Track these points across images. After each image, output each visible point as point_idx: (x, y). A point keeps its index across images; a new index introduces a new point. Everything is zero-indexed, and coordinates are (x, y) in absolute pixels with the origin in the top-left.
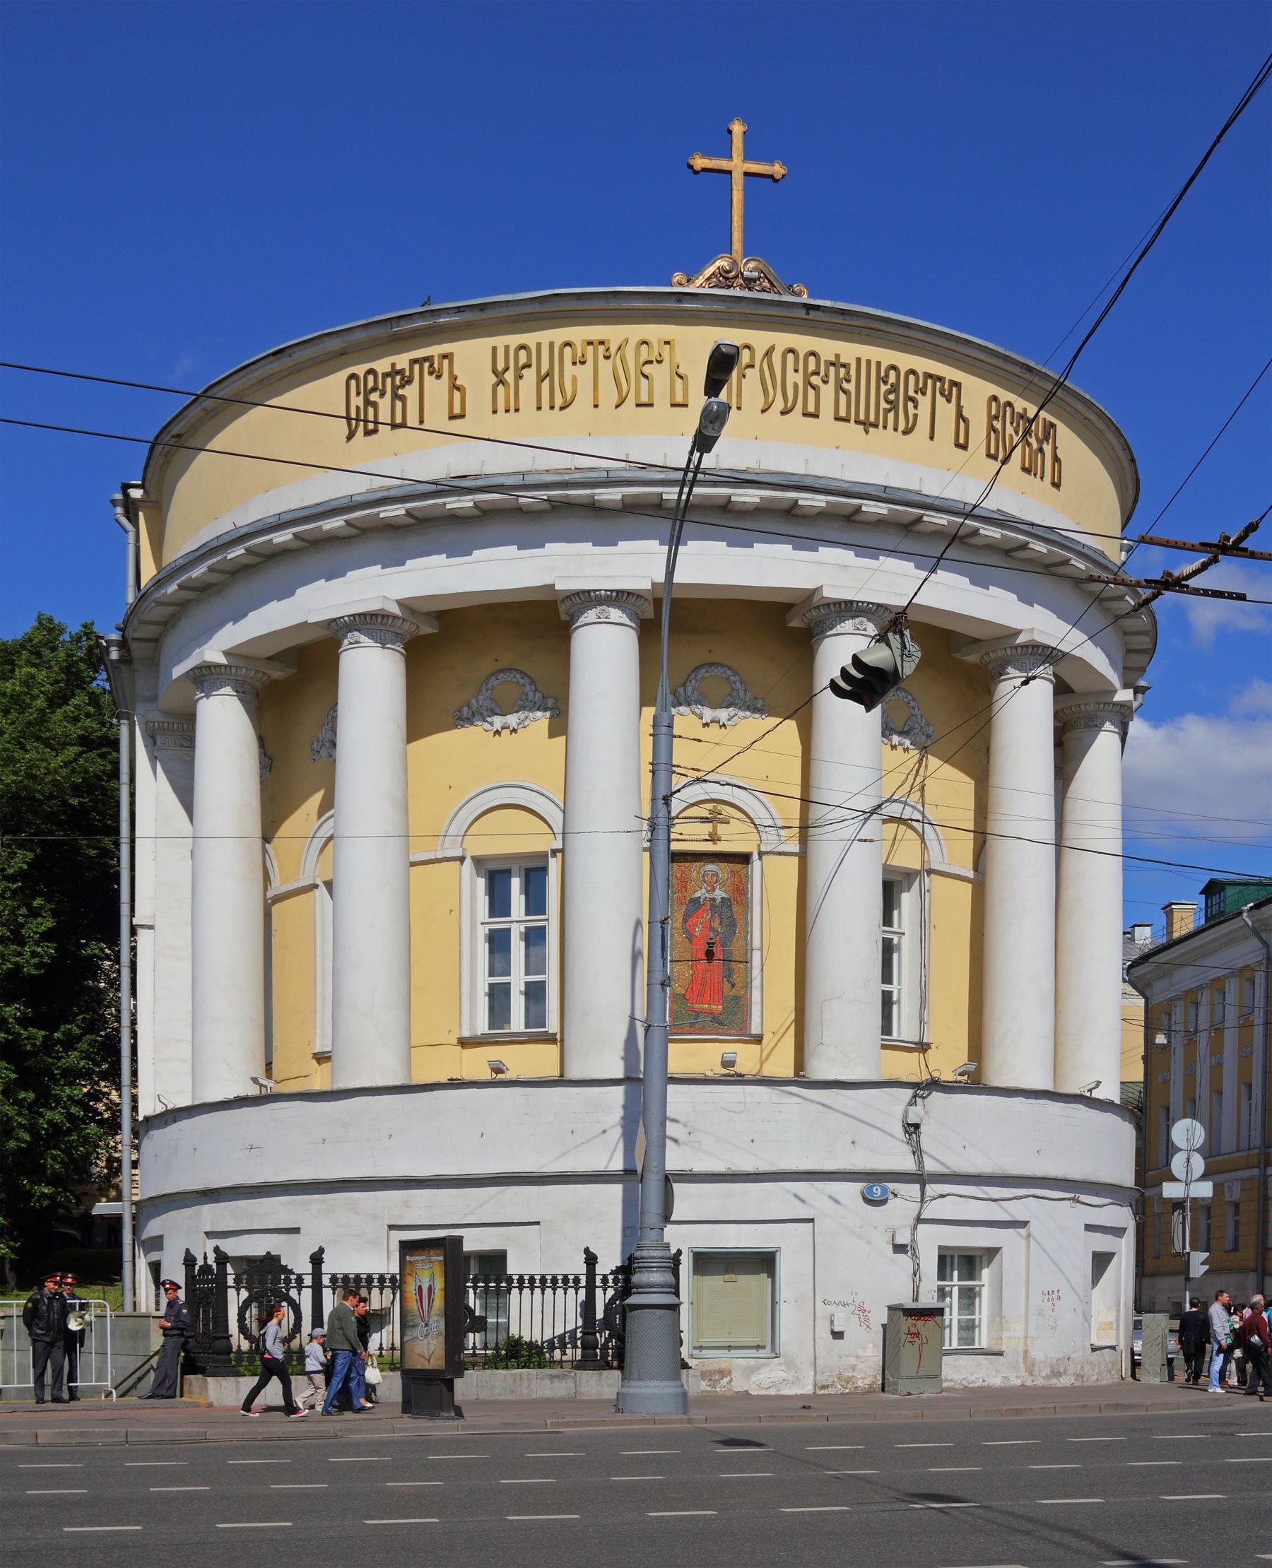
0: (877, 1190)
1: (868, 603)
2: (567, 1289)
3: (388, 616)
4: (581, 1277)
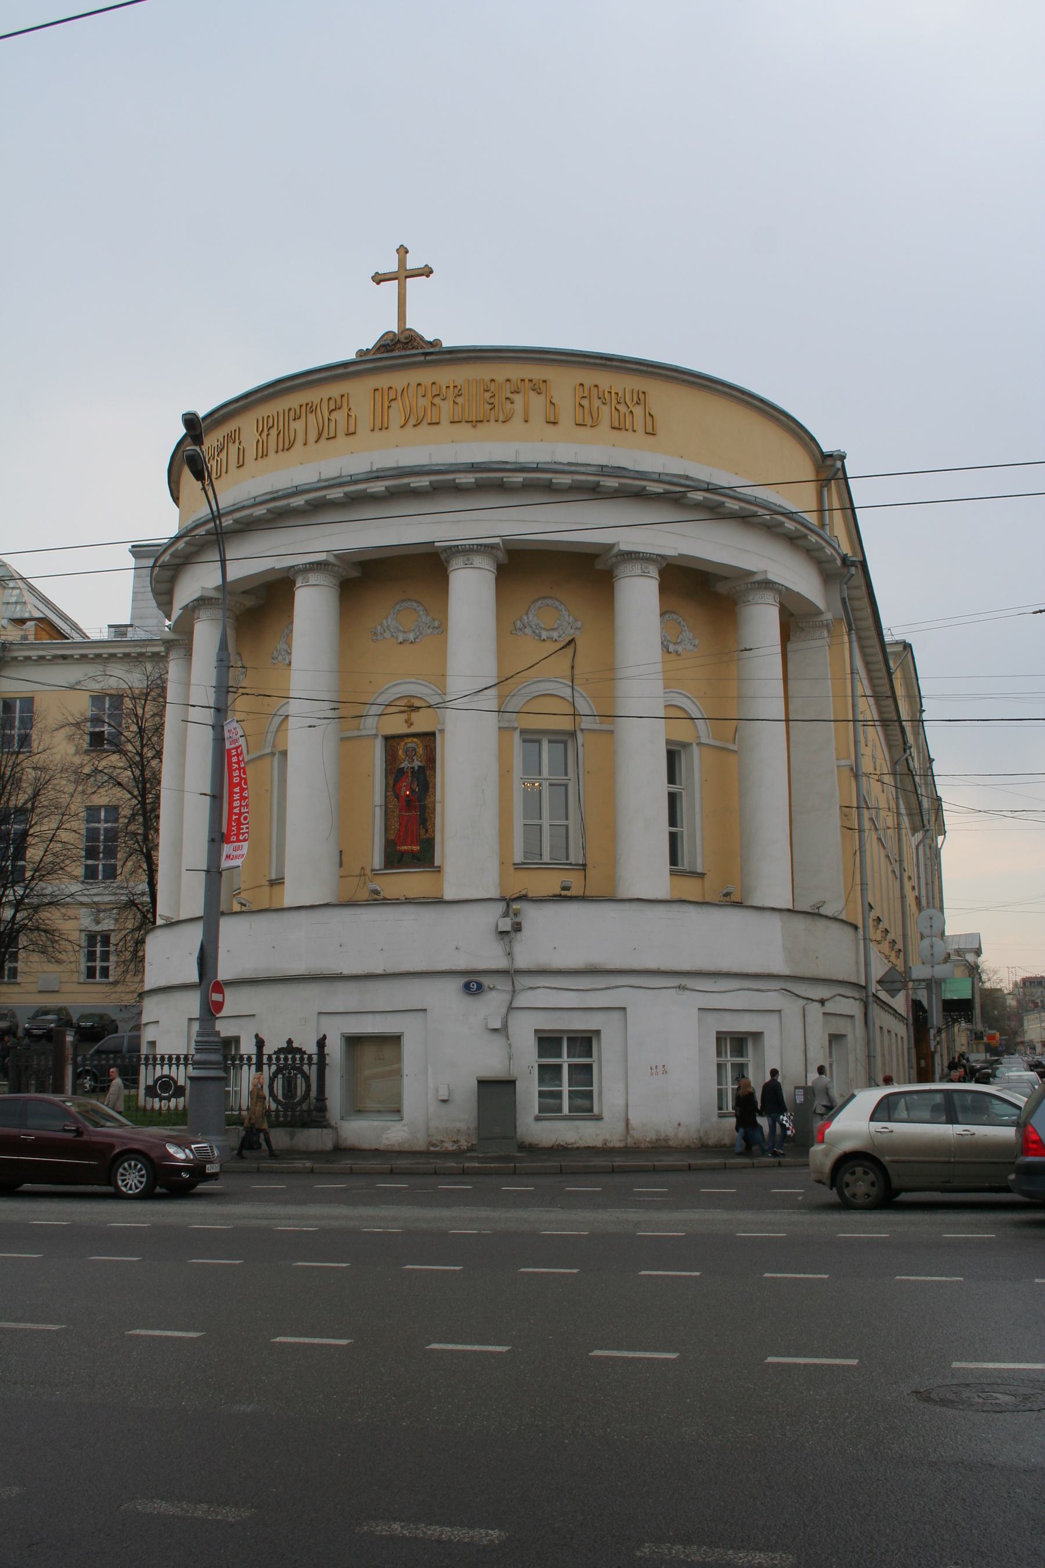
0: (473, 985)
1: (650, 554)
2: (242, 1065)
3: (329, 564)
4: (252, 1056)
